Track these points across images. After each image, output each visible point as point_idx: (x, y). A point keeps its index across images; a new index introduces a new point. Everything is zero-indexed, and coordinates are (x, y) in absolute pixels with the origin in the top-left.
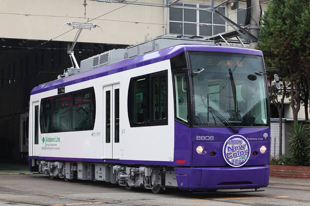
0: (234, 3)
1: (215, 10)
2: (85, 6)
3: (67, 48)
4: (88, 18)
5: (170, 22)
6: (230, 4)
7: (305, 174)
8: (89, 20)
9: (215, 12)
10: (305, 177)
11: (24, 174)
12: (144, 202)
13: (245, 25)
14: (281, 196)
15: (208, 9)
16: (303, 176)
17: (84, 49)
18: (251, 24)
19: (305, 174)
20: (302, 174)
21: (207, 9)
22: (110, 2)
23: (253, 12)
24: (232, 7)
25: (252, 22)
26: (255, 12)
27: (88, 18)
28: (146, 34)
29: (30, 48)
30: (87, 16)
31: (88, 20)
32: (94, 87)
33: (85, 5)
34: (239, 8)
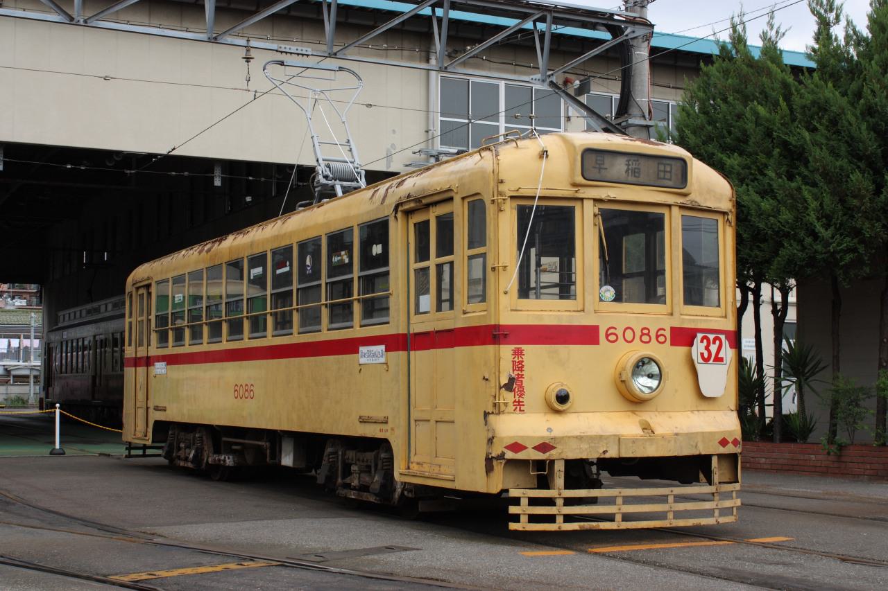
0: (581, 81)
1: (548, 80)
2: (248, 62)
3: (213, 173)
4: (254, 90)
5: (441, 121)
6: (572, 83)
7: (764, 460)
8: (258, 95)
9: (550, 85)
10: (765, 467)
11: (109, 455)
12: (391, 558)
13: (618, 118)
14: (765, 537)
15: (534, 78)
16: (759, 466)
17: (251, 176)
18: (630, 115)
19: (763, 460)
20: (757, 459)
21: (531, 77)
22: (308, 55)
23: (637, 88)
24: (575, 89)
25: (634, 111)
26: (640, 88)
27: (256, 92)
28: (389, 147)
29: (128, 172)
30: (252, 86)
31: (255, 95)
32: (518, 524)
33: (247, 58)
34: (591, 92)
